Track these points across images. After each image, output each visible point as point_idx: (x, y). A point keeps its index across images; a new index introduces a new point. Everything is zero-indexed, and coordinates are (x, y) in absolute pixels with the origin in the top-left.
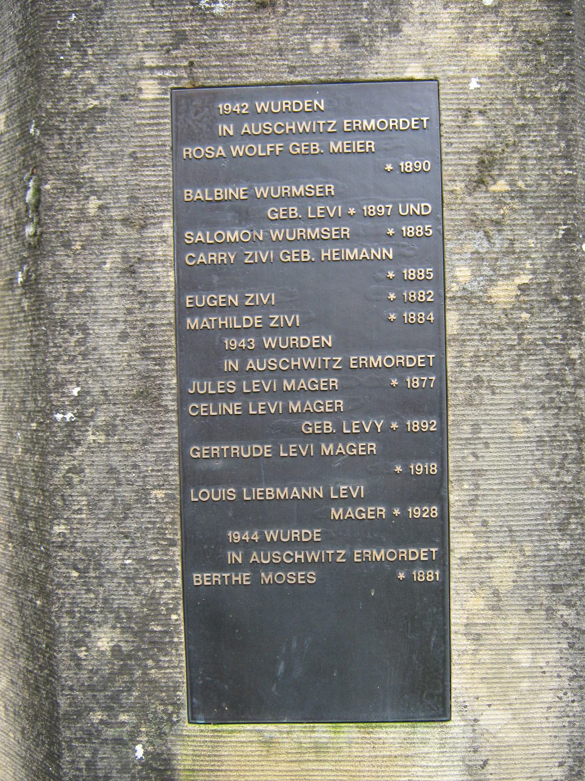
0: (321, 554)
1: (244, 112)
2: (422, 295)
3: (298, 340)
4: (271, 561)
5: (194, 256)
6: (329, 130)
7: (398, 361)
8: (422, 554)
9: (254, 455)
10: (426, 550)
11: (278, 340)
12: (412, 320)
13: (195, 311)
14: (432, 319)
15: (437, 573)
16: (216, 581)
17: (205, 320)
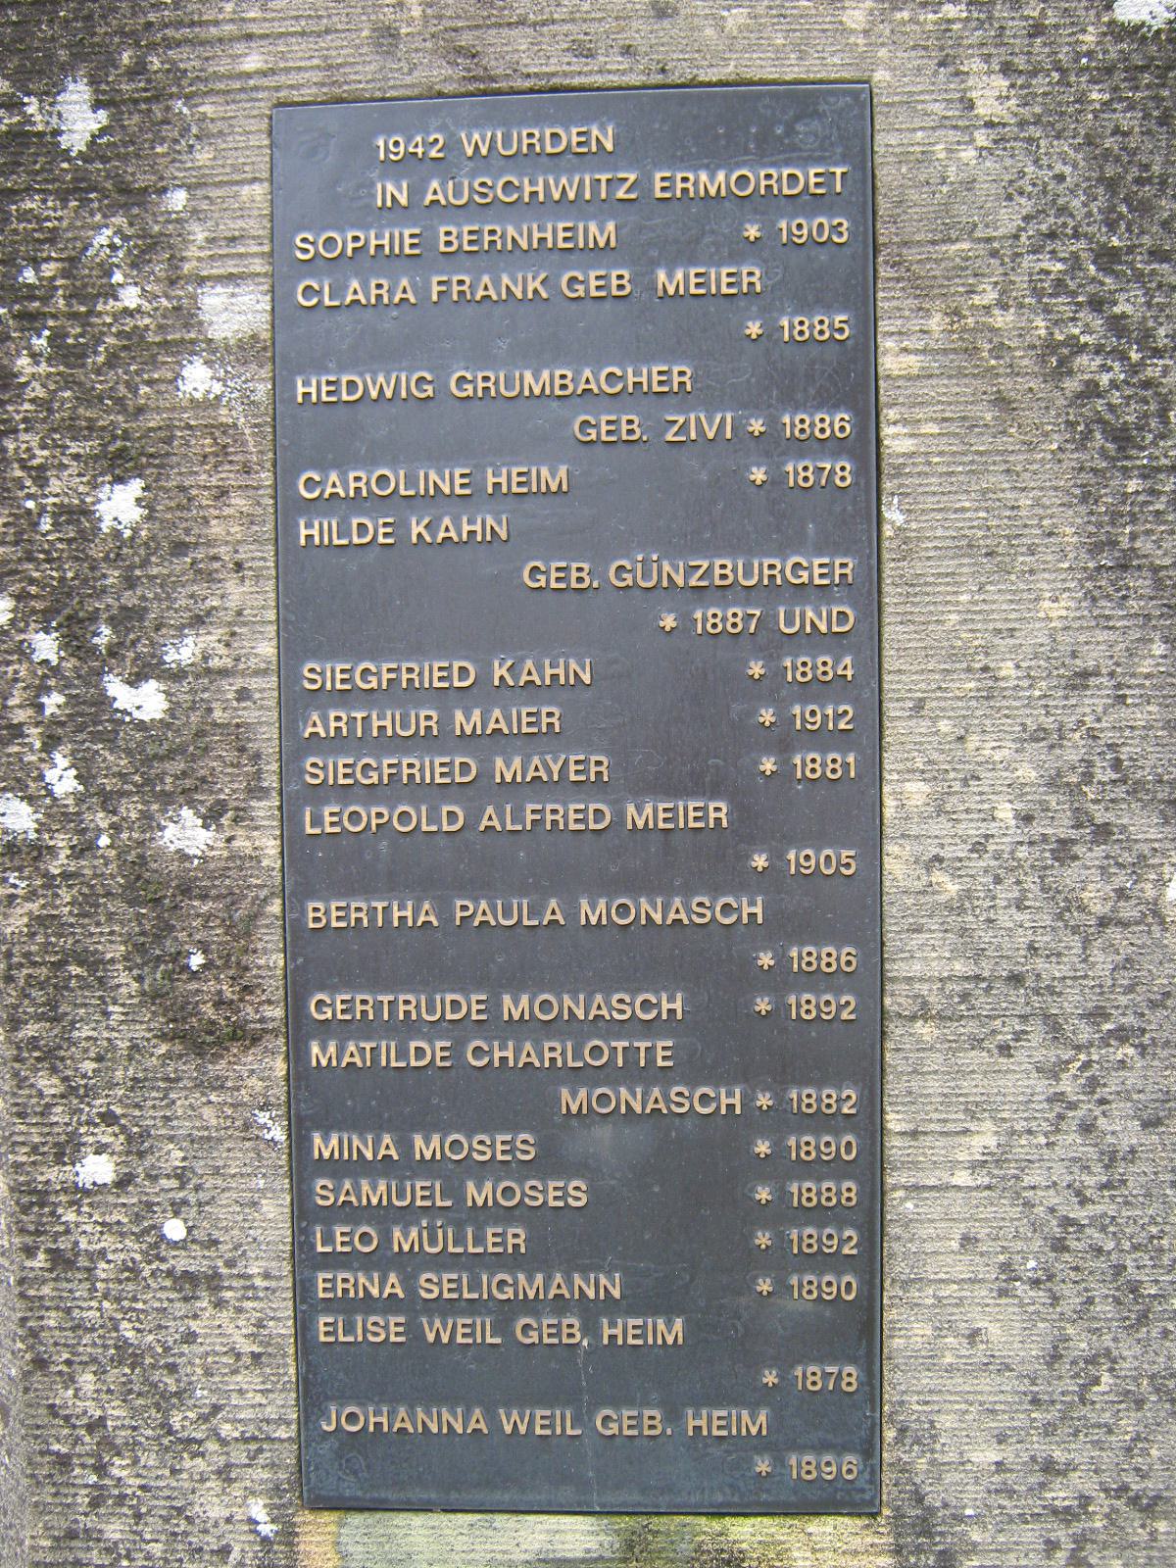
0: (581, 183)
1: (433, 154)
3: (555, 1051)
4: (470, 198)
5: (317, 478)
6: (621, 194)
7: (763, 183)
8: (815, 568)
9: (449, 1016)
12: (802, 431)
14: (849, 673)
15: (851, 759)
17: (352, 1048)
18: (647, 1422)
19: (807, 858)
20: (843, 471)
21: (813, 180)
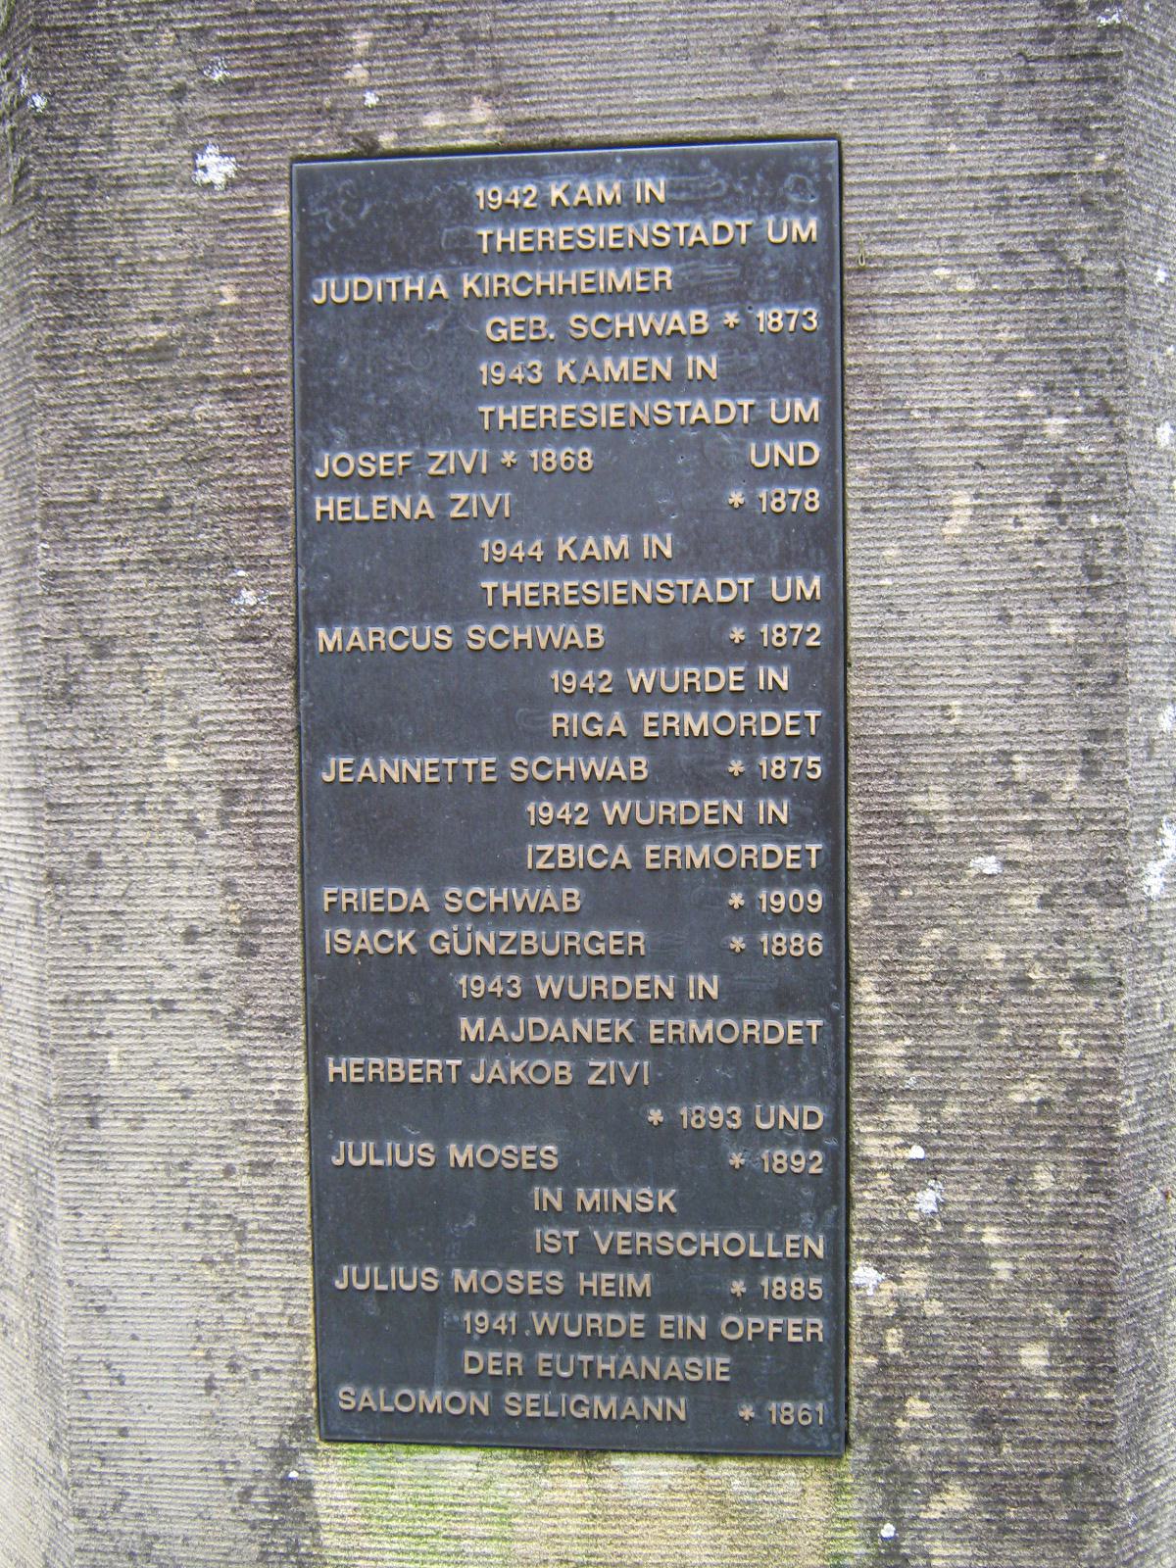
2: (795, 1286)
10: (799, 1023)
11: (561, 1319)
13: (337, 915)
16: (434, 1076)
19: (777, 897)
20: (817, 1326)
21: (789, 722)
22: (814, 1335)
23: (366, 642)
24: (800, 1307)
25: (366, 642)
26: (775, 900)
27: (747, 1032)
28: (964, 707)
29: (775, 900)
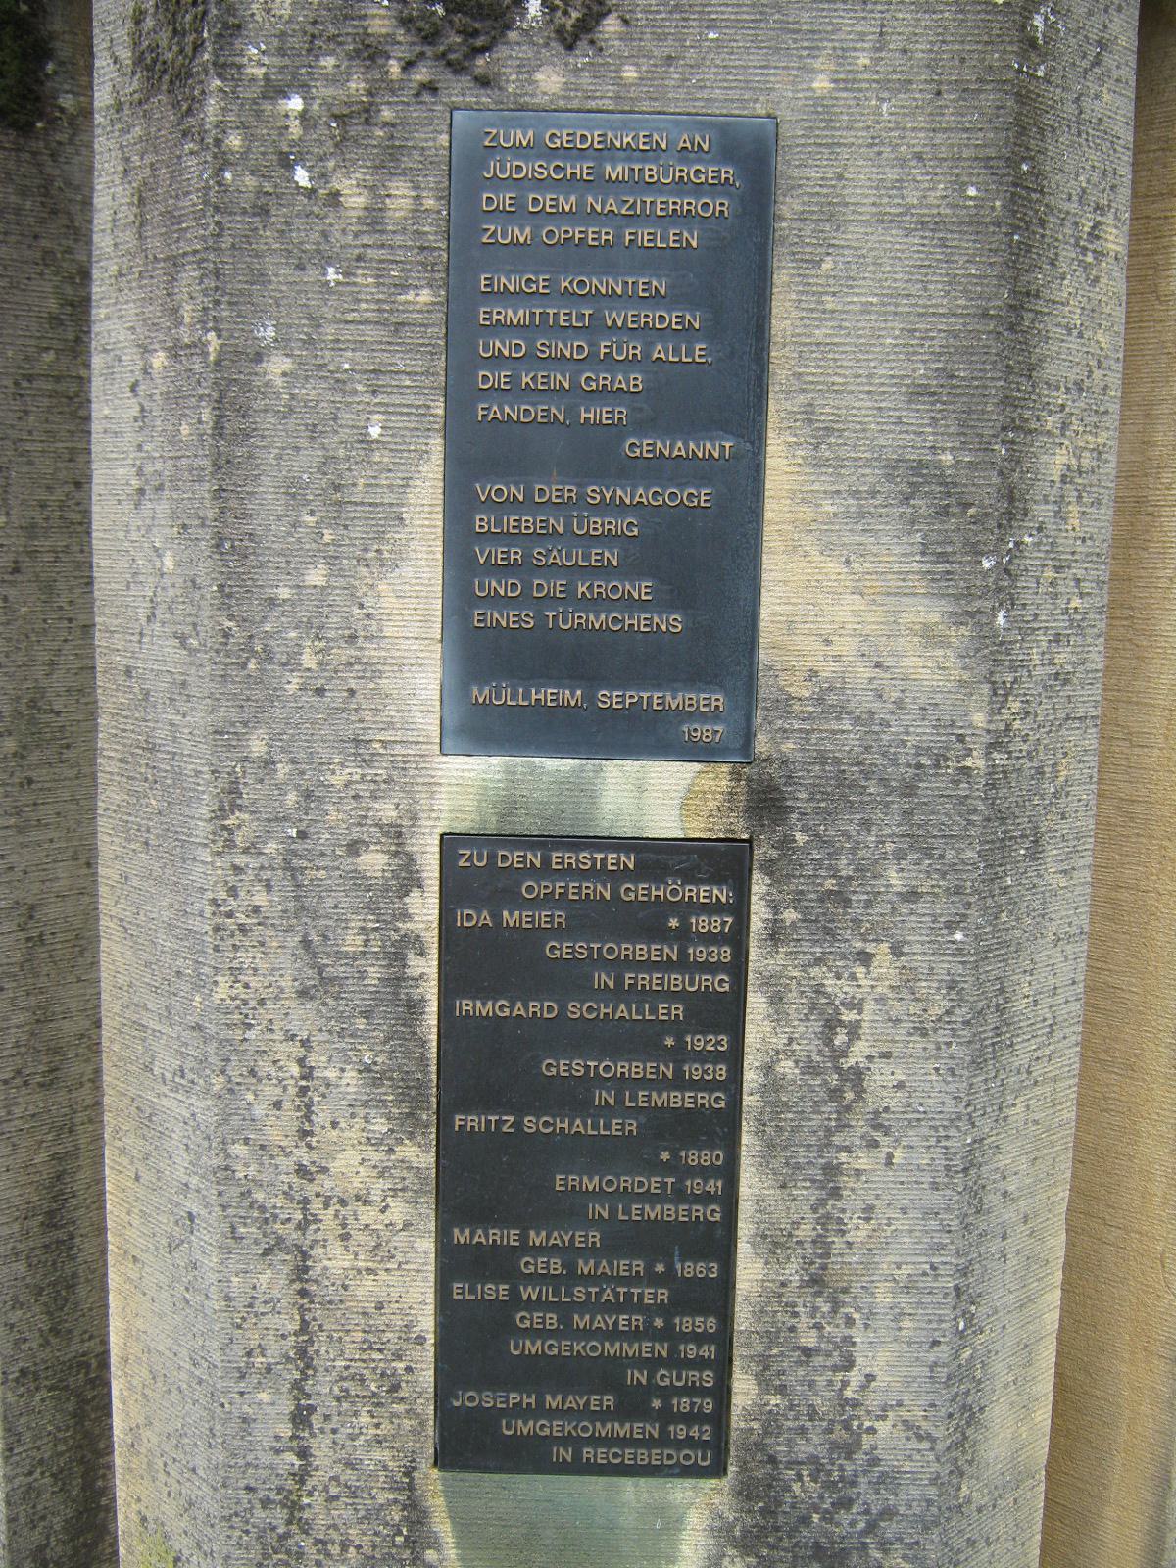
18: (552, 1266)
22: (594, 1243)
23: (527, 1011)
24: (711, 968)
25: (527, 1011)
26: (701, 923)
27: (623, 1185)
28: (983, 412)
29: (701, 923)
